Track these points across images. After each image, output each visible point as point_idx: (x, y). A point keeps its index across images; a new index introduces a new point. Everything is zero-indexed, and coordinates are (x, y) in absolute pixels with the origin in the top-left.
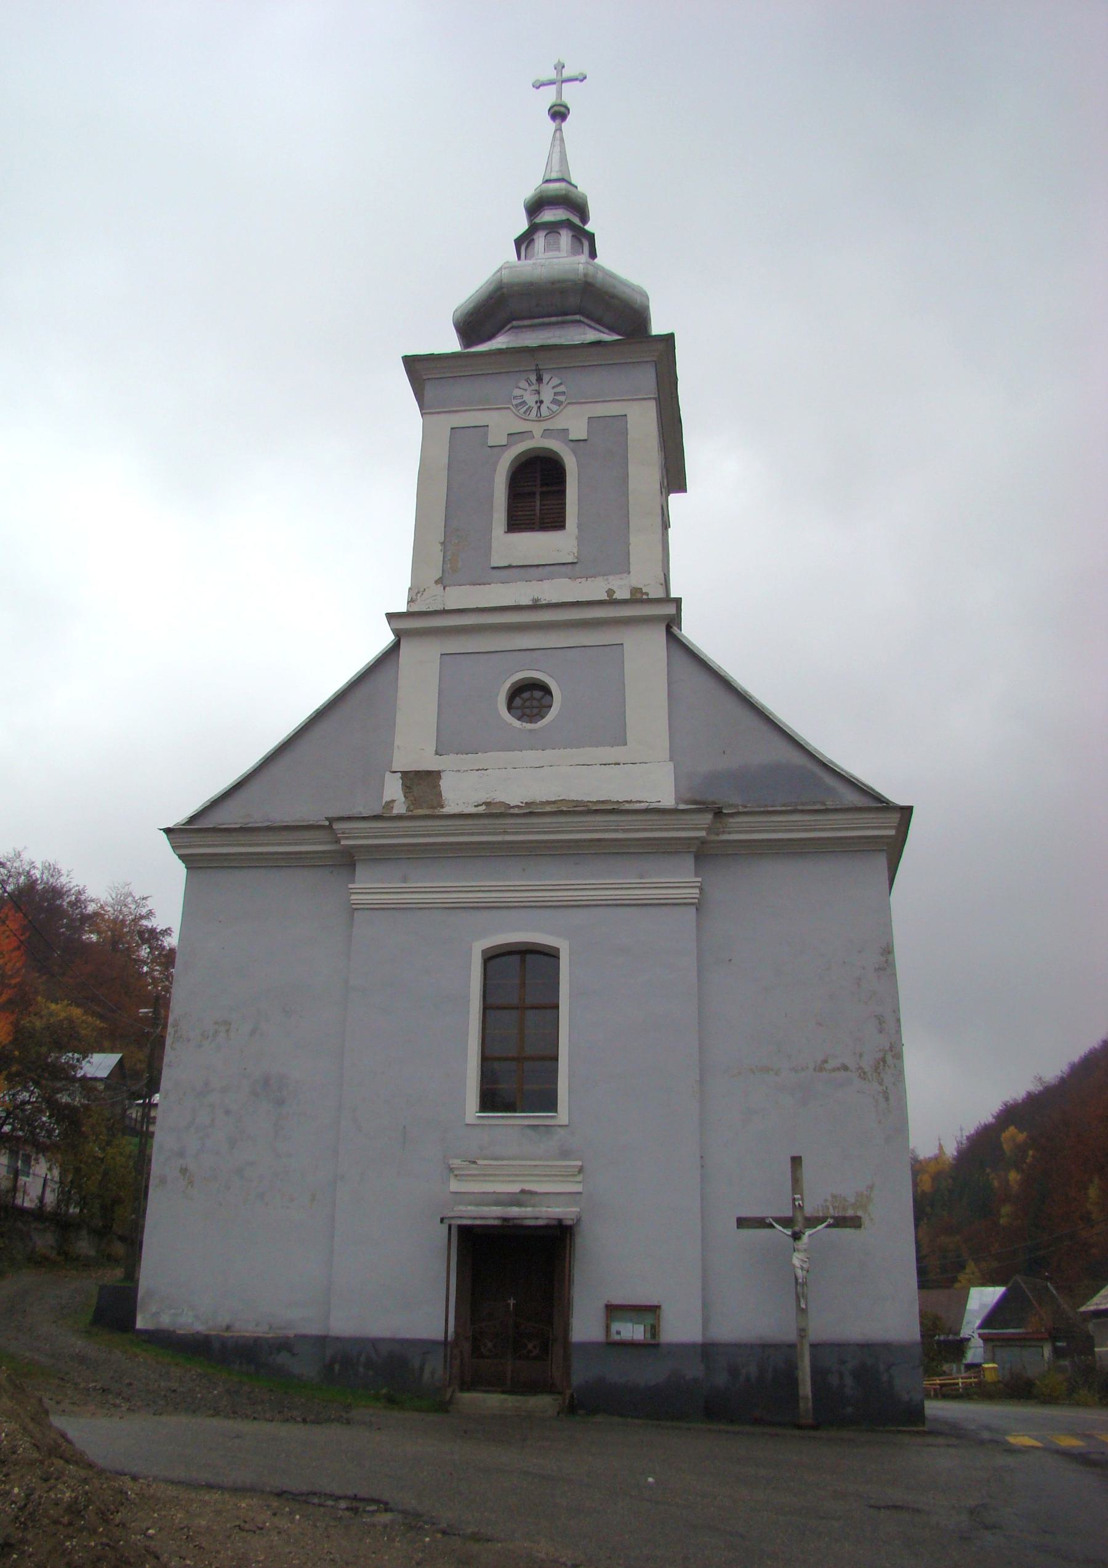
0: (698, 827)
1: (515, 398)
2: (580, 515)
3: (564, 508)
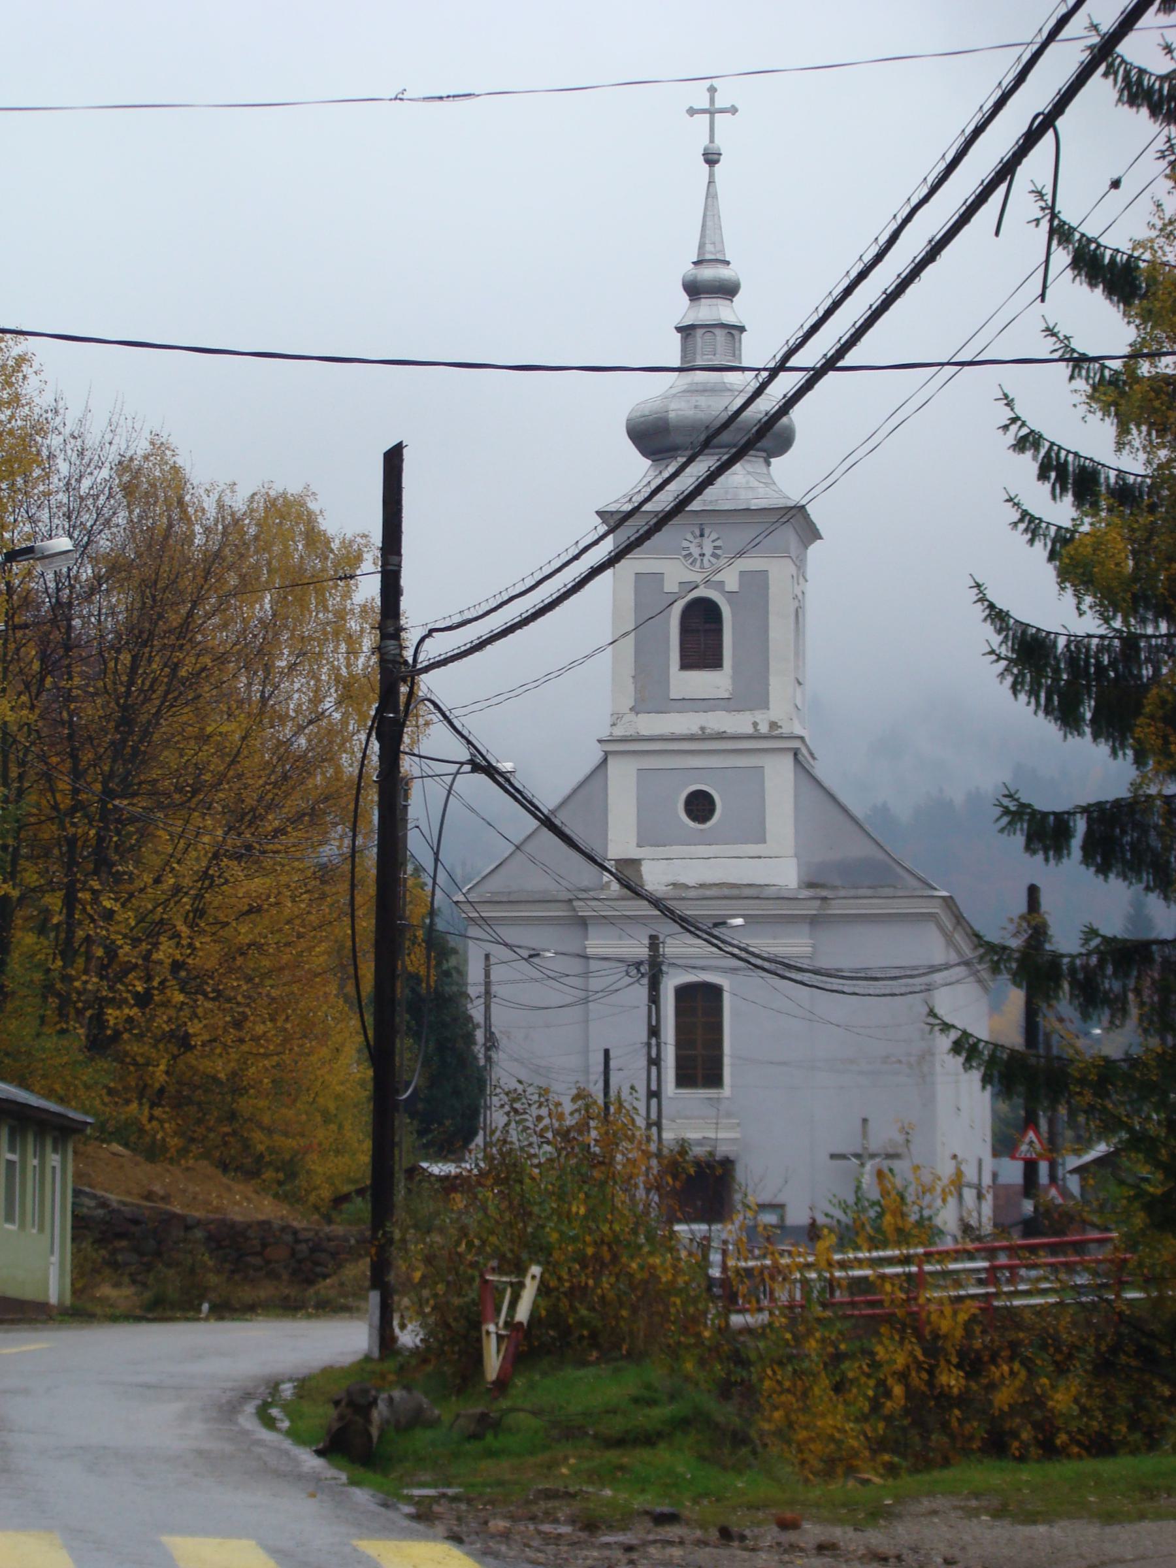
0: (812, 909)
2: (734, 656)
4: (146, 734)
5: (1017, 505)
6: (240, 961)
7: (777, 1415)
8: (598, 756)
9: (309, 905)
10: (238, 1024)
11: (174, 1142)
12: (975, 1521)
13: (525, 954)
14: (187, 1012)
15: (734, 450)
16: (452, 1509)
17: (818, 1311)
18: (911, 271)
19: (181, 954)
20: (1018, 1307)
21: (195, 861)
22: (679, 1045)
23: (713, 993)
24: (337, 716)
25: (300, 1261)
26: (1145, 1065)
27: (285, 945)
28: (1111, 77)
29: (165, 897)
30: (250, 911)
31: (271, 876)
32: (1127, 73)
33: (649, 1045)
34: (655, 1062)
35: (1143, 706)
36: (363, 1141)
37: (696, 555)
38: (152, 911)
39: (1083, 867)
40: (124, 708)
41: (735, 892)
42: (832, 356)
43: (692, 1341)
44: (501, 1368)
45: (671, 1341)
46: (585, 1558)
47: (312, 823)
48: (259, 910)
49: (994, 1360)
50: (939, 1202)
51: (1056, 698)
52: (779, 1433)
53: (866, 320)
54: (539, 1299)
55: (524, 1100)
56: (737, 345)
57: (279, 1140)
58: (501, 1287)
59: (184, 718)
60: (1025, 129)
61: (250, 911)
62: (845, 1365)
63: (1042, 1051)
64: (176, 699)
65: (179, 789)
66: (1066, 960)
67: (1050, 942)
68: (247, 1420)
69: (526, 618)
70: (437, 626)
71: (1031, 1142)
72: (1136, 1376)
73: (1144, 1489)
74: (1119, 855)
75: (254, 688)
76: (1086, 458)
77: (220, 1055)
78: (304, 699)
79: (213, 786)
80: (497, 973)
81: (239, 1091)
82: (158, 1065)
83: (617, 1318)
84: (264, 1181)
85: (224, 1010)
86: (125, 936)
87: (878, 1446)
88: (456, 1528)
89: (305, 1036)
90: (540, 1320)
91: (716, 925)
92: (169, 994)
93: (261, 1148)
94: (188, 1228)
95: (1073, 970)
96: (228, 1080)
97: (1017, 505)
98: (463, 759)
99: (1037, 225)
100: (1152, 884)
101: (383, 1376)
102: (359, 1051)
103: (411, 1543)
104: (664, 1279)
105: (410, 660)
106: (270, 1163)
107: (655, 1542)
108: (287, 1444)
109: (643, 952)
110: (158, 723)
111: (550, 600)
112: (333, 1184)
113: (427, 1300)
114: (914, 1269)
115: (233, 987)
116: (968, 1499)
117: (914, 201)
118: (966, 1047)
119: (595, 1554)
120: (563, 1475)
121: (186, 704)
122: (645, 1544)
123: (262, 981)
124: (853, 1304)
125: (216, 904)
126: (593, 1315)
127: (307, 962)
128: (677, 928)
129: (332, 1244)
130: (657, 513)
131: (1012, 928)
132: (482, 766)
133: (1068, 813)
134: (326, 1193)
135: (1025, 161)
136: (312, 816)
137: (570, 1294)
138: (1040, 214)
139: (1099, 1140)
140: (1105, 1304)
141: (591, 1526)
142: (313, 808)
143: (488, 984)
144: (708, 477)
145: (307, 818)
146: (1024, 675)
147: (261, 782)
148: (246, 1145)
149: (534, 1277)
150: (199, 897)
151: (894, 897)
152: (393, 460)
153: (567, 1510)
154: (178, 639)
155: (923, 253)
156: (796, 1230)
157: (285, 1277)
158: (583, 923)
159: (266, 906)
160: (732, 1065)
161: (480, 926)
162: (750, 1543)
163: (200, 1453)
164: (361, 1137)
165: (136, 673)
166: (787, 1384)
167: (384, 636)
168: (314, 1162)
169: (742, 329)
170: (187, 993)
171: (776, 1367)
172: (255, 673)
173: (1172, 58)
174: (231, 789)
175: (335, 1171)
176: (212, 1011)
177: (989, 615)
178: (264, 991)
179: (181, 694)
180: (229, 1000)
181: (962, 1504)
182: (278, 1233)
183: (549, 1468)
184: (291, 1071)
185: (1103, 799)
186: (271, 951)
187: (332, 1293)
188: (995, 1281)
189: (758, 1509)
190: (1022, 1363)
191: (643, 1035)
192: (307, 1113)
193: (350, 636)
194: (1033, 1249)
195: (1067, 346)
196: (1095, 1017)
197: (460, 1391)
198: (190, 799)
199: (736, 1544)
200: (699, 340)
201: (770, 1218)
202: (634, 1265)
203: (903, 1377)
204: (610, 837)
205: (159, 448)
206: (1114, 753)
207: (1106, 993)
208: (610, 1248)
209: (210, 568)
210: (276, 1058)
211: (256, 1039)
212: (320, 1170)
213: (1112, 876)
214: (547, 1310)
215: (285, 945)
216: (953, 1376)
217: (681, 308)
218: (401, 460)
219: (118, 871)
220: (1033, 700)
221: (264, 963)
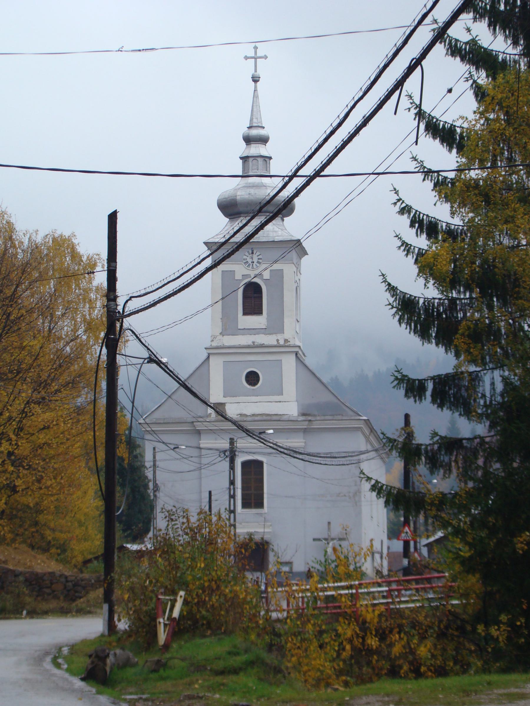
0: (305, 425)
3: (262, 301)
5: (400, 238)
6: (39, 451)
7: (294, 659)
8: (205, 356)
9: (72, 425)
10: (39, 481)
11: (9, 536)
13: (172, 447)
14: (15, 475)
15: (271, 215)
17: (311, 611)
18: (355, 131)
19: (12, 448)
20: (402, 608)
21: (19, 405)
22: (243, 489)
23: (260, 464)
24: (84, 337)
25: (69, 591)
26: (461, 496)
28: (443, 43)
29: (4, 422)
30: (44, 428)
31: (54, 412)
32: (450, 41)
33: (230, 489)
34: (232, 497)
35: (459, 330)
36: (97, 535)
37: (250, 262)
39: (432, 404)
41: (269, 418)
42: (318, 170)
43: (254, 625)
44: (166, 639)
45: (244, 626)
47: (73, 387)
48: (48, 427)
49: (391, 632)
50: (363, 560)
51: (419, 326)
52: (294, 667)
53: (334, 153)
54: (183, 607)
55: (176, 515)
56: (268, 165)
57: (58, 534)
58: (165, 601)
59: (13, 339)
60: (407, 65)
61: (44, 428)
62: (325, 636)
63: (411, 490)
64: (9, 330)
65: (11, 372)
66: (423, 447)
67: (415, 440)
68: (48, 664)
69: (176, 291)
70: (134, 295)
71: (407, 533)
72: (456, 639)
73: (464, 691)
74: (448, 399)
75: (46, 325)
76: (432, 217)
77: (31, 495)
78: (69, 329)
80: (159, 456)
81: (39, 512)
83: (219, 615)
84: (51, 554)
85: (32, 474)
87: (340, 673)
89: (70, 486)
90: (184, 616)
91: (260, 433)
92: (6, 467)
93: (50, 538)
94: (16, 576)
95: (426, 452)
96: (34, 507)
97: (400, 238)
99: (409, 111)
100: (462, 413)
101: (110, 643)
102: (96, 493)
104: (241, 597)
105: (121, 312)
106: (54, 545)
108: (67, 675)
109: (226, 445)
111: (187, 283)
112: (83, 555)
113: (131, 609)
114: (354, 591)
115: (36, 464)
116: (383, 697)
117: (356, 99)
118: (377, 488)
120: (196, 688)
121: (14, 332)
123: (50, 461)
124: (327, 608)
125: (28, 425)
126: (208, 614)
127: (71, 452)
128: (245, 435)
129: (83, 582)
130: (237, 243)
131: (397, 433)
132: (153, 359)
133: (425, 380)
134: (80, 559)
135: (407, 80)
136: (73, 384)
138: (410, 106)
139: (440, 530)
140: (442, 607)
142: (73, 380)
143: (154, 461)
144: (261, 226)
145: (70, 385)
146: (404, 316)
147: (49, 368)
148: (43, 537)
149: (181, 597)
150: (20, 422)
152: (113, 218)
155: (361, 122)
156: (299, 574)
157: (62, 598)
158: (199, 433)
159: (52, 426)
160: (268, 498)
161: (151, 434)
163: (26, 680)
164: (96, 532)
166: (298, 645)
167: (109, 300)
168: (74, 545)
169: (270, 158)
171: (293, 637)
172: (46, 317)
173: (470, 34)
174: (35, 371)
175: (84, 548)
177: (388, 288)
179: (11, 327)
180: (35, 470)
181: (381, 699)
182: (58, 578)
183: (189, 685)
184: (64, 502)
185: (441, 373)
187: (84, 605)
188: (391, 596)
190: (405, 633)
191: (227, 484)
192: (71, 522)
193: (90, 300)
194: (408, 581)
195: (422, 165)
196: (436, 473)
198: (15, 377)
200: (250, 163)
201: (286, 569)
202: (227, 591)
203: (350, 641)
204: (211, 393)
206: (446, 351)
207: (441, 462)
208: (216, 583)
209: (24, 269)
210: (56, 496)
211: (47, 488)
212: (77, 548)
213: (445, 409)
214: (187, 612)
216: (373, 641)
217: (242, 148)
218: (116, 218)
221: (50, 452)
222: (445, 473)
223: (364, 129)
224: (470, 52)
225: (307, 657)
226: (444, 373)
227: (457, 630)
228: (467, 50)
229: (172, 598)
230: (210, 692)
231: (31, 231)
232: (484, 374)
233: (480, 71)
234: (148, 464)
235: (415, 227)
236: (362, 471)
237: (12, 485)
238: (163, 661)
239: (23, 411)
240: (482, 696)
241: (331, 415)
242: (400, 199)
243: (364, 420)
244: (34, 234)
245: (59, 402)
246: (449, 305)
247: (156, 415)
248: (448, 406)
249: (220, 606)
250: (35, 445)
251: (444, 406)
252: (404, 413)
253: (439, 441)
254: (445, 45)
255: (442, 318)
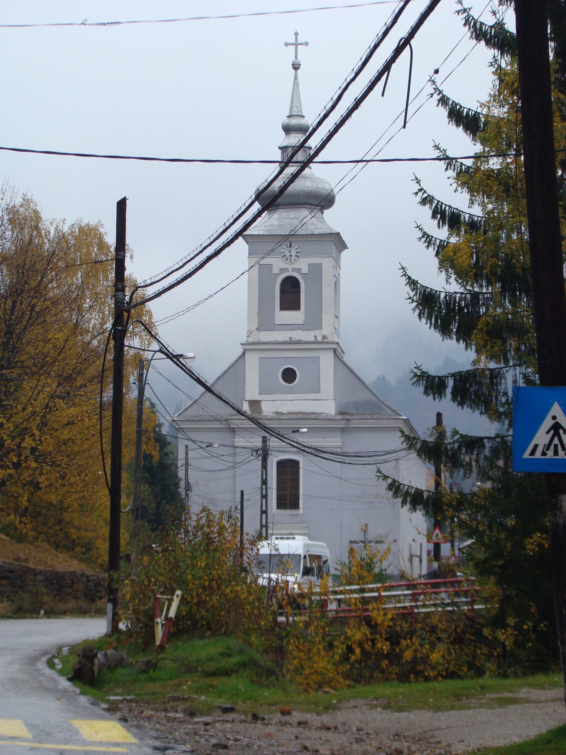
0: (342, 424)
1: (282, 253)
4: (19, 338)
5: (421, 229)
6: (63, 447)
7: (295, 662)
10: (63, 477)
11: (32, 534)
12: (374, 710)
14: (38, 472)
16: (129, 706)
18: (347, 114)
21: (42, 400)
22: (278, 489)
23: (296, 464)
25: (90, 591)
27: (85, 440)
28: (468, 26)
29: (28, 417)
30: (69, 424)
32: (475, 24)
33: (262, 489)
34: (264, 497)
38: (21, 424)
39: (452, 402)
40: (9, 326)
41: (305, 416)
43: (256, 627)
46: (185, 729)
48: (73, 423)
54: (182, 607)
57: (83, 533)
60: (396, 46)
61: (69, 424)
64: (33, 322)
65: (35, 365)
67: (447, 439)
68: (42, 665)
69: (179, 281)
72: (473, 644)
73: (456, 695)
76: (454, 208)
79: (51, 364)
80: (191, 454)
81: (63, 509)
82: (24, 497)
83: (220, 615)
84: (76, 552)
86: (8, 435)
88: (126, 715)
92: (29, 463)
93: (74, 537)
97: (421, 229)
98: (156, 350)
100: (483, 411)
103: (100, 721)
106: (79, 544)
107: (220, 721)
109: (259, 444)
110: (24, 333)
111: (189, 272)
116: (372, 700)
117: (348, 80)
119: (190, 726)
120: (184, 690)
122: (215, 722)
123: (74, 457)
125: (52, 420)
126: (208, 614)
131: (429, 433)
133: (445, 376)
137: (198, 604)
141: (192, 714)
143: (187, 459)
147: (74, 362)
148: (67, 536)
149: (178, 596)
150: (44, 416)
151: (381, 419)
153: (183, 706)
154: (35, 293)
159: (76, 421)
162: (266, 721)
163: (12, 679)
165: (14, 309)
167: (117, 290)
168: (100, 544)
170: (38, 463)
171: (294, 639)
176: (50, 471)
177: (408, 282)
178: (75, 462)
180: (59, 466)
181: (369, 703)
182: (79, 577)
183: (178, 686)
185: (461, 370)
186: (78, 442)
189: (273, 705)
197: (144, 650)
198: (39, 370)
199: (259, 722)
203: (360, 645)
205: (27, 202)
209: (50, 260)
211: (71, 485)
213: (465, 407)
214: (186, 612)
215: (85, 440)
218: (126, 206)
219: (5, 404)
220: (429, 322)
221: (75, 448)
222: (465, 473)
223: (356, 112)
224: (496, 36)
225: (309, 659)
226: (465, 370)
227: (474, 635)
228: (493, 34)
229: (169, 597)
230: (197, 693)
231: (58, 220)
232: (506, 371)
233: (505, 56)
234: (181, 462)
235: (437, 218)
236: (379, 470)
237: (35, 482)
238: (153, 661)
239: (47, 406)
240: (473, 701)
241: (369, 414)
242: (422, 189)
243: (404, 419)
244: (61, 223)
245: (85, 397)
246: (471, 300)
247: (190, 412)
248: (469, 404)
249: (220, 606)
250: (59, 441)
251: (465, 404)
252: (436, 413)
253: (460, 440)
254: (470, 28)
255: (464, 312)
